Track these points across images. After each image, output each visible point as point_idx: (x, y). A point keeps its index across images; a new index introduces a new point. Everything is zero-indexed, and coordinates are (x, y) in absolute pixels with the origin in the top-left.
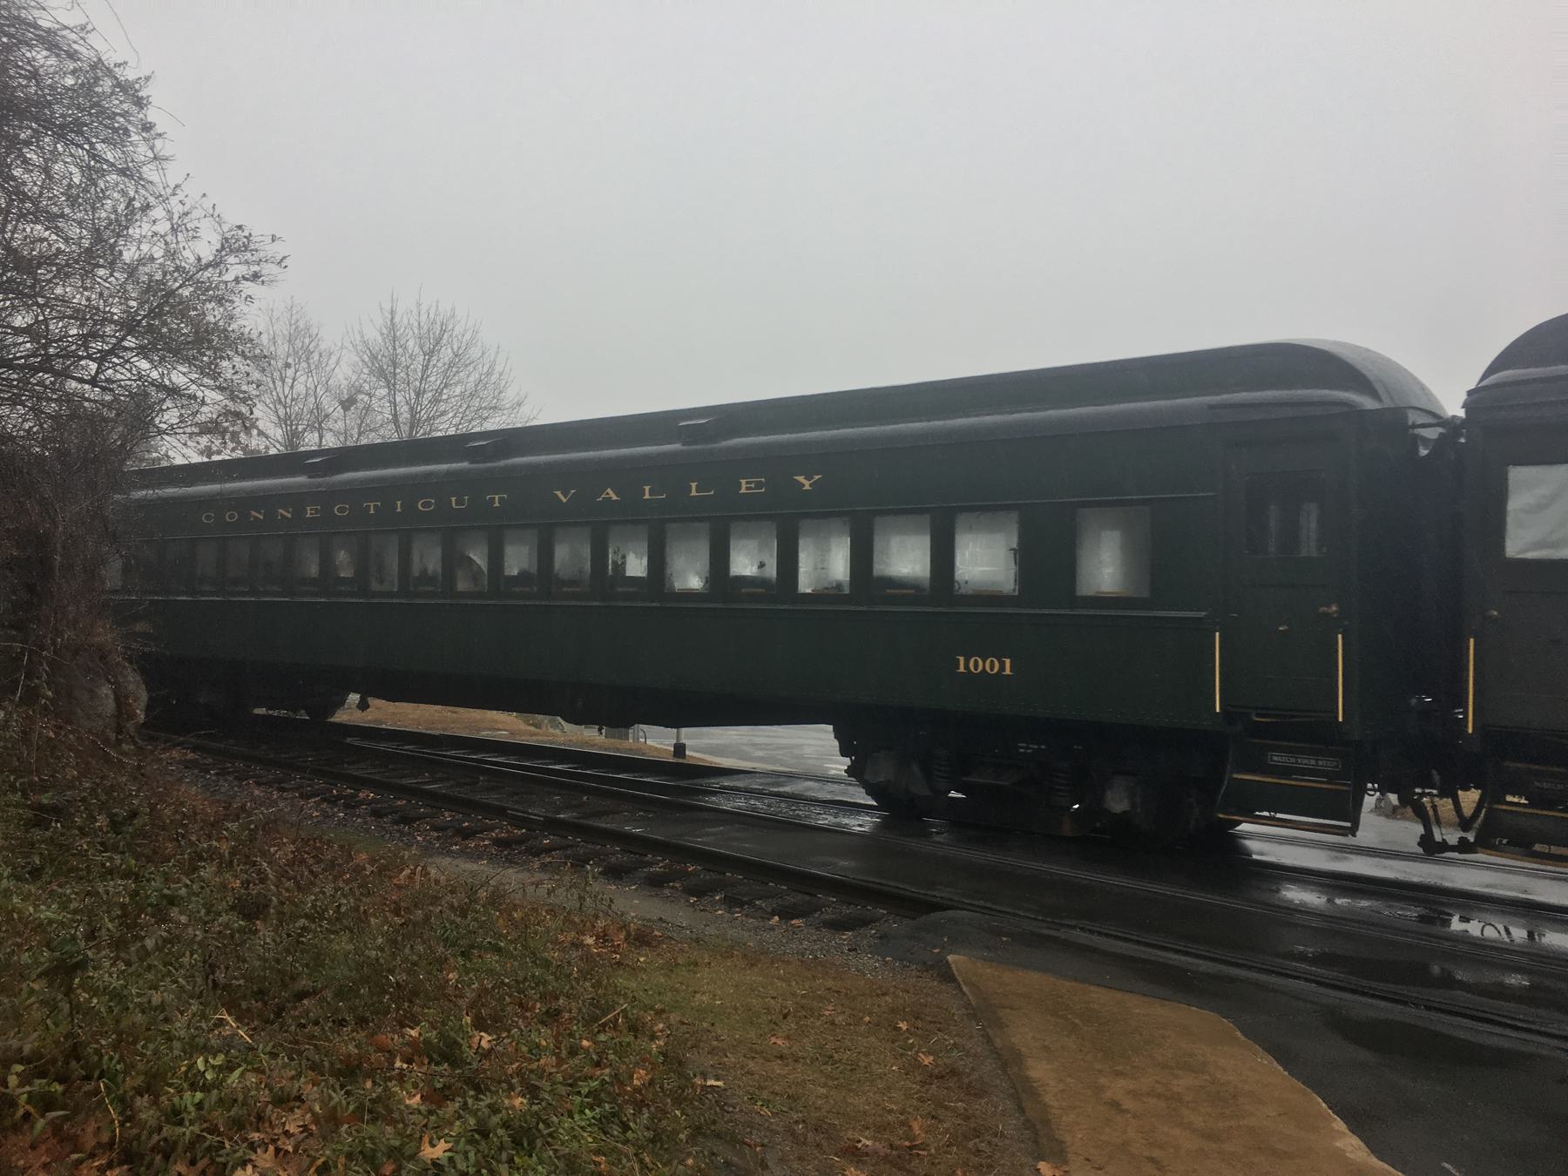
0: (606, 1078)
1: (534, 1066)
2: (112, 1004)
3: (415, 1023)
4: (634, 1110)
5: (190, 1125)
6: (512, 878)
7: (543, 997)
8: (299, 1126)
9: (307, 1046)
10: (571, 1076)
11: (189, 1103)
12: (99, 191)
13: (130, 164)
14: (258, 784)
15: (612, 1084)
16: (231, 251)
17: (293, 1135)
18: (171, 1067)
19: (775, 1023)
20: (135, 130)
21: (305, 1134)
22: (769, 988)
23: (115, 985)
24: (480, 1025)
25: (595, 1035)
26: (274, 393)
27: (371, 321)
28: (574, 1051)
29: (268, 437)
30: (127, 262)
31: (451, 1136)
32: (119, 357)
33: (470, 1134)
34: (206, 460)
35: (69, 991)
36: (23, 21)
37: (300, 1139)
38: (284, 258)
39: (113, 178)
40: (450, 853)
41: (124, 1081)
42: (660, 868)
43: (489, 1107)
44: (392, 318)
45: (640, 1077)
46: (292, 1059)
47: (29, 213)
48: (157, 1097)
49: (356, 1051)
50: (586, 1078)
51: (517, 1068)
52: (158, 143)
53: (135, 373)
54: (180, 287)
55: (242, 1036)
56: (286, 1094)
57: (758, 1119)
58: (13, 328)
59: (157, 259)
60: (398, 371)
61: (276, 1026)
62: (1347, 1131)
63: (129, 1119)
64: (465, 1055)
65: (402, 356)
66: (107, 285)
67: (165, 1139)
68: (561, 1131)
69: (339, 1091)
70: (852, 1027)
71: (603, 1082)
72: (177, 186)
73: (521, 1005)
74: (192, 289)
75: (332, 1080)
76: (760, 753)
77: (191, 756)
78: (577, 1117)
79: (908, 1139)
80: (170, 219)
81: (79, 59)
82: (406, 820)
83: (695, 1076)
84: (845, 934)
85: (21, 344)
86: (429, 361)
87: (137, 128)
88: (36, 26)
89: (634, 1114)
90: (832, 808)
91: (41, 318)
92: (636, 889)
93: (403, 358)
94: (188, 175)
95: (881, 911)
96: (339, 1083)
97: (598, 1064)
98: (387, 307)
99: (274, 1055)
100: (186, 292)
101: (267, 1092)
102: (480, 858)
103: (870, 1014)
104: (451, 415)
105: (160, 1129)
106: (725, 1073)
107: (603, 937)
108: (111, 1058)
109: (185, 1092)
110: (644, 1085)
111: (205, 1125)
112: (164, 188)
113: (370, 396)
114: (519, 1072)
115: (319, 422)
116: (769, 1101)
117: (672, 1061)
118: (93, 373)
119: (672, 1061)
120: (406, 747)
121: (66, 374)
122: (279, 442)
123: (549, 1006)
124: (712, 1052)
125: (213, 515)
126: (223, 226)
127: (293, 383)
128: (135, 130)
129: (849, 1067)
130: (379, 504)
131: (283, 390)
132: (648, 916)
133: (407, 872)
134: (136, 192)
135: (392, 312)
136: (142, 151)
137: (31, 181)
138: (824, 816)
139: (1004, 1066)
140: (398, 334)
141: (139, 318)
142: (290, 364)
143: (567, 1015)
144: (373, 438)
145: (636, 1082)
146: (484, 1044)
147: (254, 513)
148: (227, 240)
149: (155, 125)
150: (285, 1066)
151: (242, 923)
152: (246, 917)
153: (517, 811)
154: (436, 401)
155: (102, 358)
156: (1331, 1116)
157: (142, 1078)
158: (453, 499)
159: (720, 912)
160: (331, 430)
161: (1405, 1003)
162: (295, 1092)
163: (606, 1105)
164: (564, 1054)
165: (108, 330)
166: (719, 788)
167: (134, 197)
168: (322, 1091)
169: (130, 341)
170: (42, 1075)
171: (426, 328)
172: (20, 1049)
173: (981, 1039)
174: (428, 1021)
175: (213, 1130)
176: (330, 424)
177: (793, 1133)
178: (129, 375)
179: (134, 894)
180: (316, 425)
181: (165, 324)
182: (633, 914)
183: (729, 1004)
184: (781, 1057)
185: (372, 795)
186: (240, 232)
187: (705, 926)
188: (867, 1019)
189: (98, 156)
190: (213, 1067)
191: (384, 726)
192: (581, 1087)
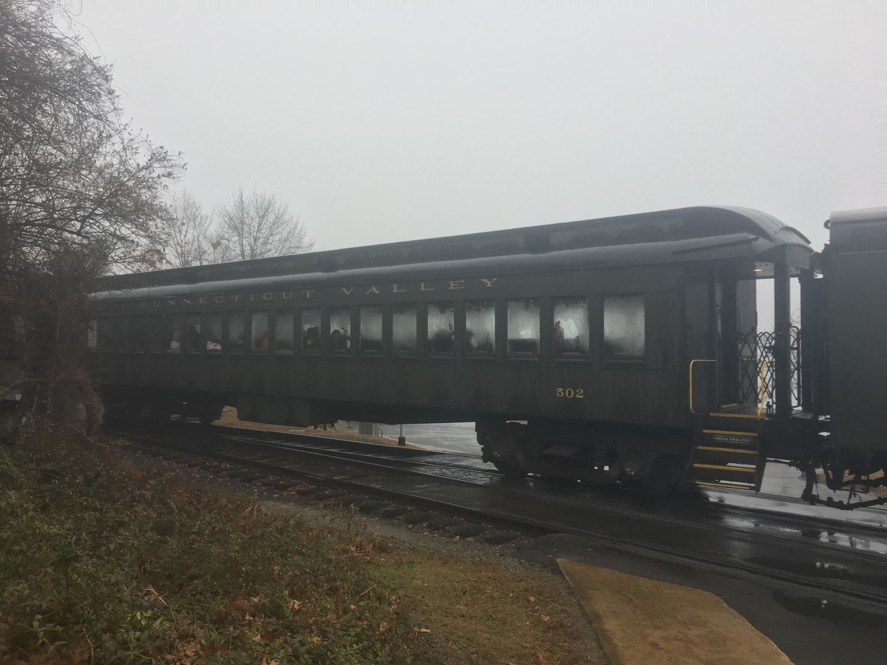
0: (365, 627)
1: (324, 619)
2: (89, 582)
3: (256, 594)
4: (380, 645)
5: (133, 650)
6: (309, 514)
7: (327, 581)
9: (197, 607)
10: (345, 625)
11: (132, 637)
12: (84, 127)
13: (101, 113)
14: (165, 459)
15: (368, 630)
16: (156, 160)
17: (190, 657)
18: (122, 617)
19: (459, 597)
20: (104, 94)
21: (197, 656)
23: (91, 570)
24: (293, 595)
26: (175, 240)
27: (228, 203)
28: (345, 612)
30: (98, 167)
31: (278, 658)
32: (93, 219)
35: (66, 574)
36: (44, 34)
37: (194, 659)
38: (185, 164)
39: (92, 120)
40: (273, 499)
41: (96, 625)
42: (392, 508)
44: (242, 197)
45: (383, 626)
47: (45, 140)
48: (115, 634)
49: (225, 610)
50: (353, 627)
51: (315, 620)
53: (101, 228)
54: (128, 180)
55: (161, 600)
56: (186, 633)
57: (450, 651)
58: (35, 203)
59: (115, 165)
60: (244, 227)
61: (179, 595)
62: (789, 661)
63: (99, 647)
66: (87, 179)
67: (119, 658)
68: (340, 656)
69: (215, 631)
70: (502, 600)
73: (316, 585)
74: (134, 182)
75: (211, 626)
76: (447, 443)
78: (348, 649)
80: (123, 143)
81: (74, 55)
83: (414, 626)
84: (497, 546)
85: (39, 212)
86: (262, 221)
87: (105, 93)
88: (51, 37)
89: (381, 647)
90: (489, 474)
91: (51, 198)
92: (378, 520)
93: (247, 220)
94: (132, 118)
95: (518, 533)
96: (215, 628)
97: (360, 619)
98: (238, 194)
99: (179, 612)
101: (175, 632)
102: (290, 501)
103: (513, 592)
104: (273, 251)
105: (117, 652)
106: (431, 625)
107: (360, 547)
108: (89, 612)
110: (386, 631)
111: (141, 651)
113: (228, 240)
114: (315, 623)
115: (200, 253)
116: (457, 641)
117: (401, 617)
118: (78, 228)
119: (401, 617)
123: (331, 585)
124: (423, 613)
126: (152, 146)
128: (104, 94)
131: (180, 238)
133: (249, 509)
134: (104, 128)
136: (107, 105)
137: (46, 122)
138: (485, 479)
139: (590, 623)
140: (245, 206)
141: (105, 197)
143: (342, 591)
145: (381, 629)
146: (296, 606)
147: (174, 304)
148: (154, 154)
149: (115, 91)
151: (159, 537)
153: (309, 474)
154: (265, 243)
155: (83, 220)
156: (780, 652)
157: (106, 623)
159: (426, 533)
161: (821, 588)
163: (365, 641)
164: (340, 613)
165: (88, 204)
166: (425, 463)
167: (103, 131)
168: (206, 632)
170: (50, 621)
172: (40, 607)
173: (577, 607)
174: (263, 593)
175: (146, 653)
177: (471, 660)
178: (98, 229)
179: (99, 521)
180: (199, 257)
181: (119, 201)
182: (377, 534)
183: (432, 586)
184: (463, 616)
185: (229, 465)
186: (161, 150)
187: (417, 541)
188: (511, 595)
189: (83, 108)
190: (146, 618)
191: (235, 427)
192: (351, 631)
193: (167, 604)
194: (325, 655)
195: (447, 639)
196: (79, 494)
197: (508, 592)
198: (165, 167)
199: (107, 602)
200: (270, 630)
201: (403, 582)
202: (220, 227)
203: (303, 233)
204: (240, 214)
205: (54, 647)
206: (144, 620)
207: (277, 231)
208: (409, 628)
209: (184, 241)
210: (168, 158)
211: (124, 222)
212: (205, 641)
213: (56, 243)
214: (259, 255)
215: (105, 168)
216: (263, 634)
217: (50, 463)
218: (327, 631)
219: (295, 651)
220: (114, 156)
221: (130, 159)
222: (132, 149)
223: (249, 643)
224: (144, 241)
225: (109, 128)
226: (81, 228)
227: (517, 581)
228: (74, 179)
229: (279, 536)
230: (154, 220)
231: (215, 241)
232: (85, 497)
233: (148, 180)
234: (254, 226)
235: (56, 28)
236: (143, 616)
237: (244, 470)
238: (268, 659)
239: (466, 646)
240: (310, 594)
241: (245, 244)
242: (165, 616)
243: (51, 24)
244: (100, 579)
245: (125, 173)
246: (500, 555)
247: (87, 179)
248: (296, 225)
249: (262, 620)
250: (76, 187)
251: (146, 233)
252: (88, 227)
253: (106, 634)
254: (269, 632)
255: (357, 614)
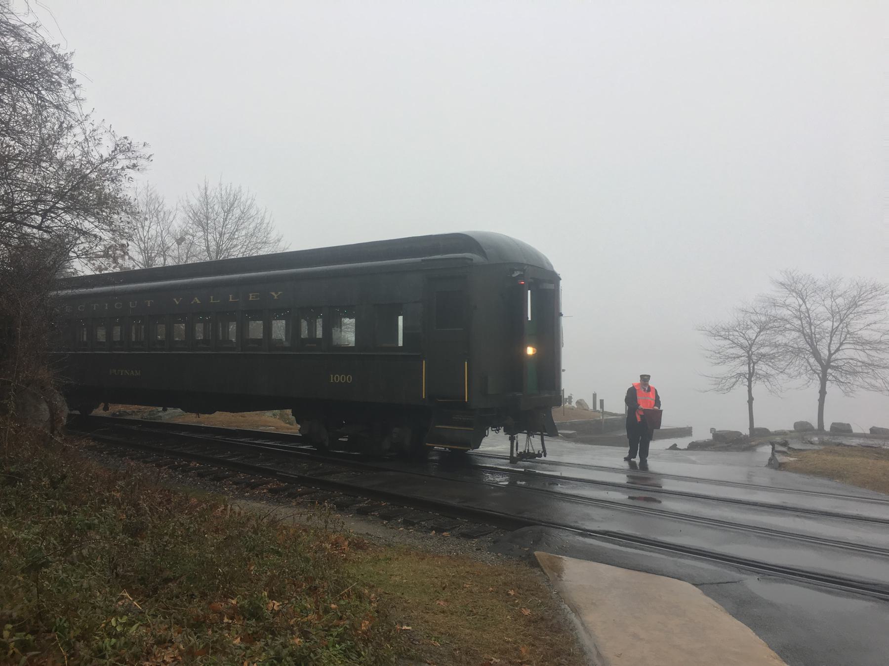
0: (348, 626)
1: (305, 620)
2: (59, 588)
3: (233, 595)
4: (363, 644)
8: (172, 658)
9: (174, 611)
10: (326, 626)
11: (107, 645)
13: (61, 103)
14: (133, 459)
15: (351, 630)
16: (120, 152)
19: (438, 592)
21: (176, 662)
22: (433, 572)
24: (271, 596)
25: (338, 601)
26: (138, 235)
28: (327, 611)
29: (135, 259)
31: (260, 662)
33: (271, 660)
34: (98, 273)
35: (36, 581)
38: (151, 155)
41: (69, 633)
43: (282, 645)
44: (206, 192)
45: (365, 625)
46: (165, 618)
49: (203, 613)
50: (336, 626)
52: (78, 91)
53: (63, 222)
54: (91, 172)
55: (135, 605)
57: (433, 648)
60: (209, 222)
63: (72, 655)
64: (265, 614)
65: (211, 213)
66: (48, 172)
68: (323, 657)
71: (346, 629)
72: (87, 115)
75: (189, 630)
77: (92, 444)
78: (331, 649)
79: (519, 658)
80: (85, 134)
82: (219, 479)
84: (473, 541)
86: (227, 216)
88: (6, 23)
92: (352, 517)
94: (94, 109)
98: (203, 186)
99: (155, 616)
100: (93, 176)
102: (261, 500)
103: (492, 586)
104: (240, 247)
107: (336, 544)
108: (61, 620)
109: (105, 638)
111: (117, 658)
112: (81, 116)
113: (193, 236)
114: (297, 624)
115: (164, 251)
118: (39, 222)
120: (216, 437)
121: (22, 223)
122: (140, 263)
124: (404, 609)
125: (121, 304)
127: (149, 229)
128: (64, 83)
129: (483, 617)
130: (153, 301)
131: (142, 233)
132: (360, 532)
134: (65, 118)
135: (206, 189)
141: (66, 191)
142: (147, 218)
143: (321, 590)
144: (194, 260)
148: (118, 145)
149: (76, 80)
150: (161, 623)
151: (130, 539)
152: (132, 536)
153: (282, 472)
154: (231, 239)
155: (44, 215)
157: (80, 631)
158: (131, 303)
159: (401, 529)
160: (170, 256)
162: (169, 638)
164: (321, 613)
165: (49, 197)
167: (64, 121)
168: (184, 637)
169: (61, 204)
170: (20, 629)
171: (225, 198)
172: (11, 616)
174: (241, 594)
176: (170, 253)
177: (454, 656)
178: (59, 224)
180: (162, 253)
181: (81, 194)
183: (411, 582)
184: (443, 612)
188: (491, 589)
189: (43, 98)
190: (121, 624)
193: (142, 608)
194: (308, 657)
195: (429, 636)
196: (45, 497)
197: (487, 587)
198: (130, 158)
199: (80, 609)
200: (250, 632)
201: (381, 579)
202: (184, 222)
203: (269, 229)
204: (205, 209)
205: (27, 658)
206: (119, 626)
207: (243, 226)
208: (391, 626)
209: (147, 237)
210: (133, 150)
211: (88, 215)
212: (183, 646)
213: (16, 238)
214: (225, 250)
215: (66, 160)
216: (242, 637)
217: (14, 465)
218: (309, 632)
219: (278, 653)
220: (76, 147)
221: (92, 150)
222: (95, 139)
223: (229, 646)
224: (107, 236)
225: (70, 119)
226: (42, 222)
227: (496, 575)
228: (34, 171)
229: (253, 536)
230: (118, 214)
231: (179, 237)
232: (52, 500)
233: (111, 172)
234: (219, 222)
235: (13, 13)
236: (118, 622)
237: (214, 469)
238: (249, 662)
239: (448, 643)
240: (289, 594)
241: (210, 240)
242: (141, 621)
243: (8, 9)
244: (72, 585)
245: (87, 165)
246: (477, 550)
247: (48, 172)
248: (263, 219)
249: (241, 622)
250: (36, 180)
251: (110, 227)
252: (49, 221)
253: (80, 642)
254: (249, 634)
255: (339, 614)
